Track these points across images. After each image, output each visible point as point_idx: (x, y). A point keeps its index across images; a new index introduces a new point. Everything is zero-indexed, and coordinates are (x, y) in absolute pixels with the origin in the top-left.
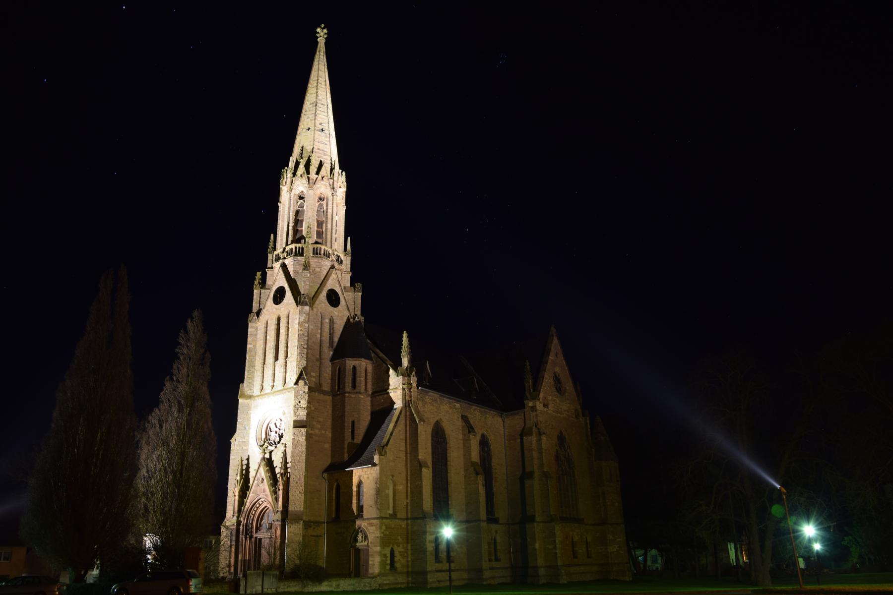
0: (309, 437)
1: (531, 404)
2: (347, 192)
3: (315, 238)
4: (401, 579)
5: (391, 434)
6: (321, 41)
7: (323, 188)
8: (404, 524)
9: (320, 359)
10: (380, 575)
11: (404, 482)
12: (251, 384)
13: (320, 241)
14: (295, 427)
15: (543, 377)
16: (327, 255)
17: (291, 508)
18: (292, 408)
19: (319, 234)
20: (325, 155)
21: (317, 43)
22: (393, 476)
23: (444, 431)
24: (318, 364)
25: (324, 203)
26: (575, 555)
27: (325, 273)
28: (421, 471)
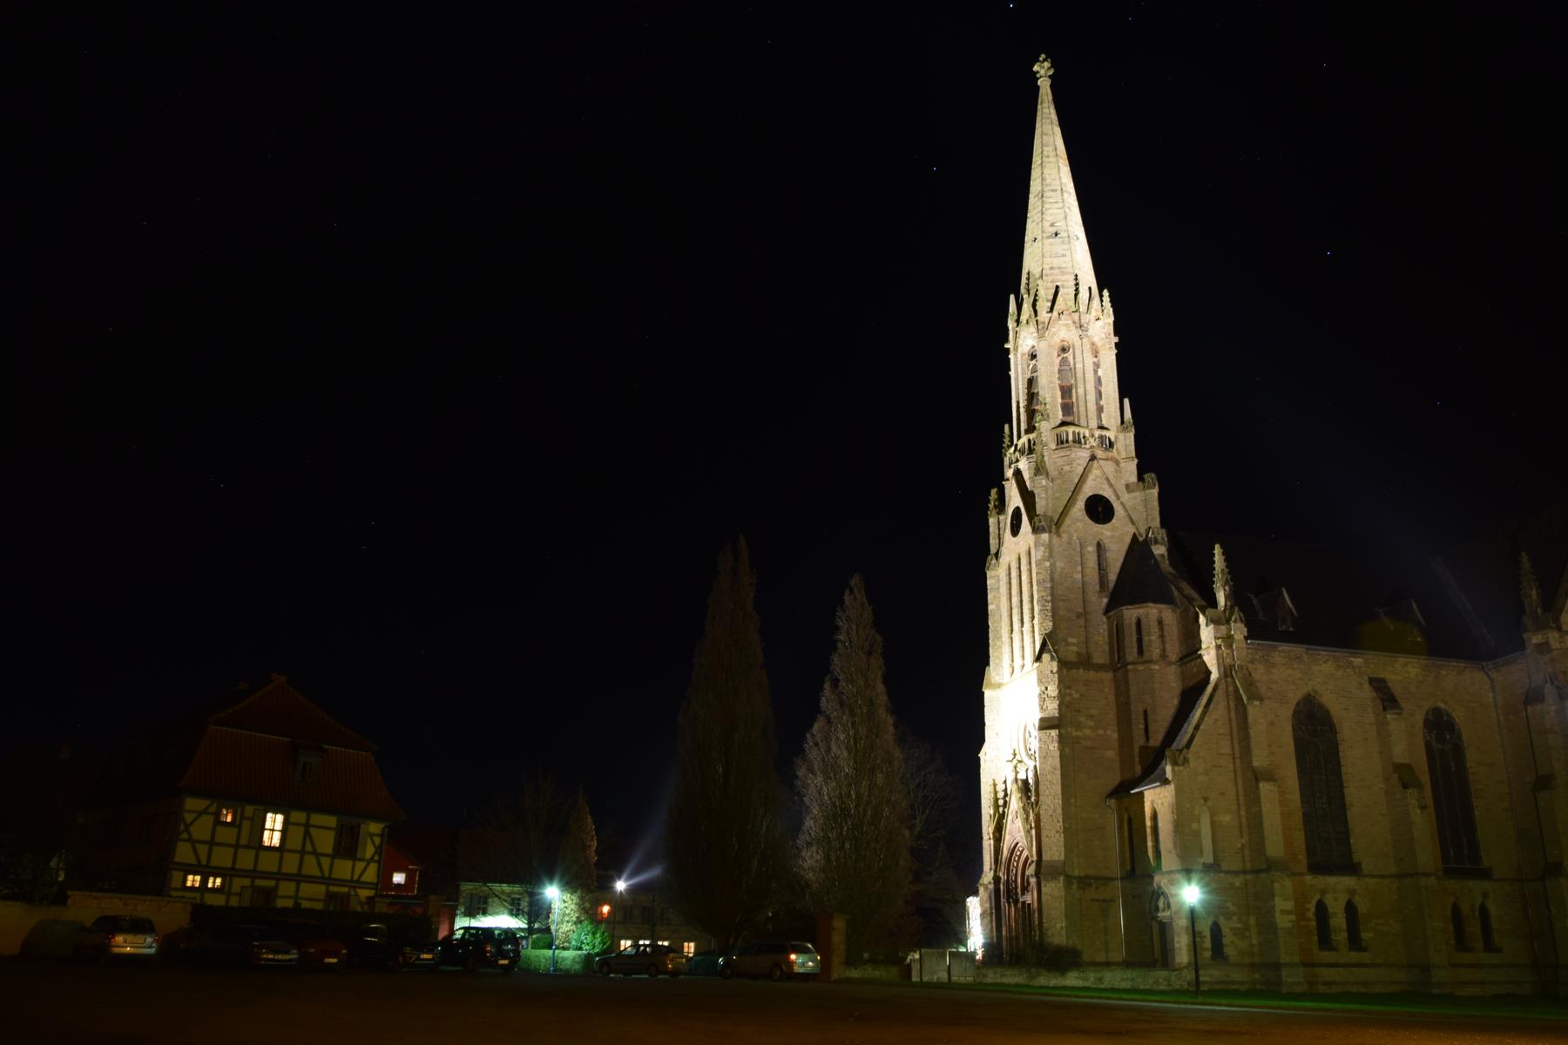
0: (1062, 740)
1: (1536, 639)
2: (1115, 323)
3: (1060, 416)
4: (1238, 976)
6: (1044, 84)
7: (1063, 331)
9: (1085, 614)
11: (1234, 808)
12: (999, 665)
13: (1069, 419)
14: (1041, 728)
16: (1078, 441)
17: (1045, 857)
18: (1036, 701)
19: (1067, 408)
20: (1063, 273)
21: (1038, 88)
22: (1206, 799)
23: (1328, 712)
24: (1082, 622)
25: (1069, 355)
27: (1080, 470)
28: (1258, 788)
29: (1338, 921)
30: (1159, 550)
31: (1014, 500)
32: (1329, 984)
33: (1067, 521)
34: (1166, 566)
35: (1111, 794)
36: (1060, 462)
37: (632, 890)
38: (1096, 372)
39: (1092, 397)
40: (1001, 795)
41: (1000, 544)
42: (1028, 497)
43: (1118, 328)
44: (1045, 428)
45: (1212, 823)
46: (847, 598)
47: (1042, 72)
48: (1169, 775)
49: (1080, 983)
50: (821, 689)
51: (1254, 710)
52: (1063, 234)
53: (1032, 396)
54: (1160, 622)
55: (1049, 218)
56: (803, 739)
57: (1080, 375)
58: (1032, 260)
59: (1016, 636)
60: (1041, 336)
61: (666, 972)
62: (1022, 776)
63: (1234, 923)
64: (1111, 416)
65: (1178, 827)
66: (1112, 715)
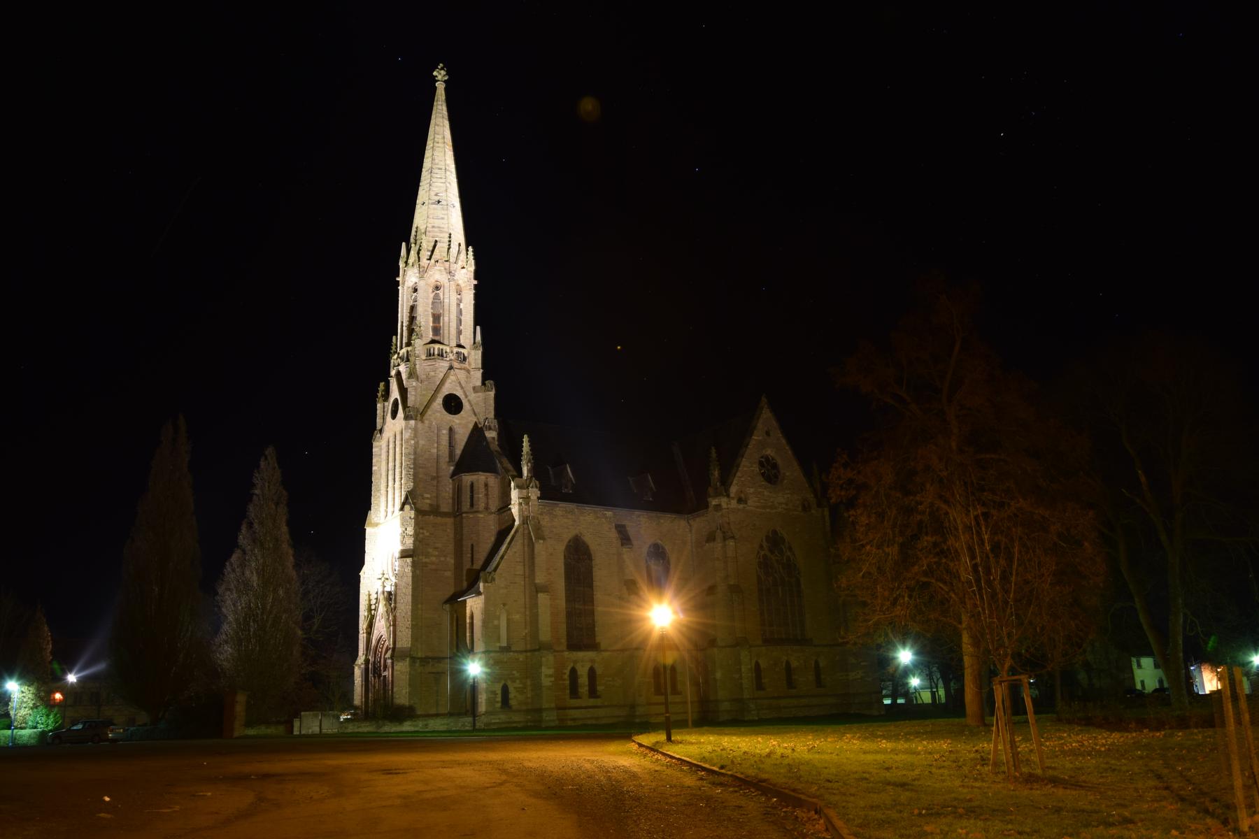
0: (414, 565)
4: (516, 718)
5: (502, 557)
6: (440, 87)
7: (437, 274)
8: (521, 657)
9: (437, 478)
10: (487, 713)
13: (437, 338)
15: (738, 466)
16: (441, 355)
18: (399, 538)
19: (436, 330)
20: (441, 232)
24: (435, 483)
25: (440, 292)
26: (790, 684)
27: (441, 375)
29: (584, 680)
30: (491, 435)
31: (395, 394)
32: (574, 720)
33: (429, 412)
34: (495, 446)
35: (446, 602)
36: (428, 369)
37: (80, 680)
38: (458, 305)
39: (454, 324)
40: (373, 602)
41: (384, 423)
42: (403, 391)
43: (477, 275)
44: (419, 344)
45: (508, 620)
46: (262, 463)
47: (440, 77)
48: (481, 589)
49: (412, 729)
50: (239, 530)
51: (539, 546)
52: (443, 202)
53: (412, 319)
54: (486, 485)
55: (435, 189)
56: (224, 566)
57: (446, 307)
58: (421, 218)
59: (390, 489)
60: (421, 277)
61: (108, 740)
62: (388, 589)
63: (518, 684)
64: (467, 339)
65: (485, 623)
66: (451, 547)
